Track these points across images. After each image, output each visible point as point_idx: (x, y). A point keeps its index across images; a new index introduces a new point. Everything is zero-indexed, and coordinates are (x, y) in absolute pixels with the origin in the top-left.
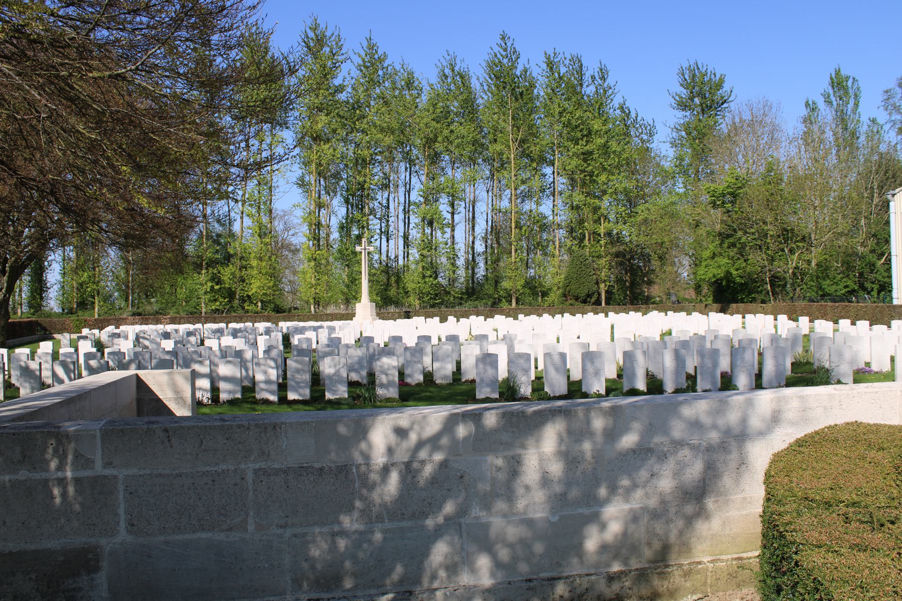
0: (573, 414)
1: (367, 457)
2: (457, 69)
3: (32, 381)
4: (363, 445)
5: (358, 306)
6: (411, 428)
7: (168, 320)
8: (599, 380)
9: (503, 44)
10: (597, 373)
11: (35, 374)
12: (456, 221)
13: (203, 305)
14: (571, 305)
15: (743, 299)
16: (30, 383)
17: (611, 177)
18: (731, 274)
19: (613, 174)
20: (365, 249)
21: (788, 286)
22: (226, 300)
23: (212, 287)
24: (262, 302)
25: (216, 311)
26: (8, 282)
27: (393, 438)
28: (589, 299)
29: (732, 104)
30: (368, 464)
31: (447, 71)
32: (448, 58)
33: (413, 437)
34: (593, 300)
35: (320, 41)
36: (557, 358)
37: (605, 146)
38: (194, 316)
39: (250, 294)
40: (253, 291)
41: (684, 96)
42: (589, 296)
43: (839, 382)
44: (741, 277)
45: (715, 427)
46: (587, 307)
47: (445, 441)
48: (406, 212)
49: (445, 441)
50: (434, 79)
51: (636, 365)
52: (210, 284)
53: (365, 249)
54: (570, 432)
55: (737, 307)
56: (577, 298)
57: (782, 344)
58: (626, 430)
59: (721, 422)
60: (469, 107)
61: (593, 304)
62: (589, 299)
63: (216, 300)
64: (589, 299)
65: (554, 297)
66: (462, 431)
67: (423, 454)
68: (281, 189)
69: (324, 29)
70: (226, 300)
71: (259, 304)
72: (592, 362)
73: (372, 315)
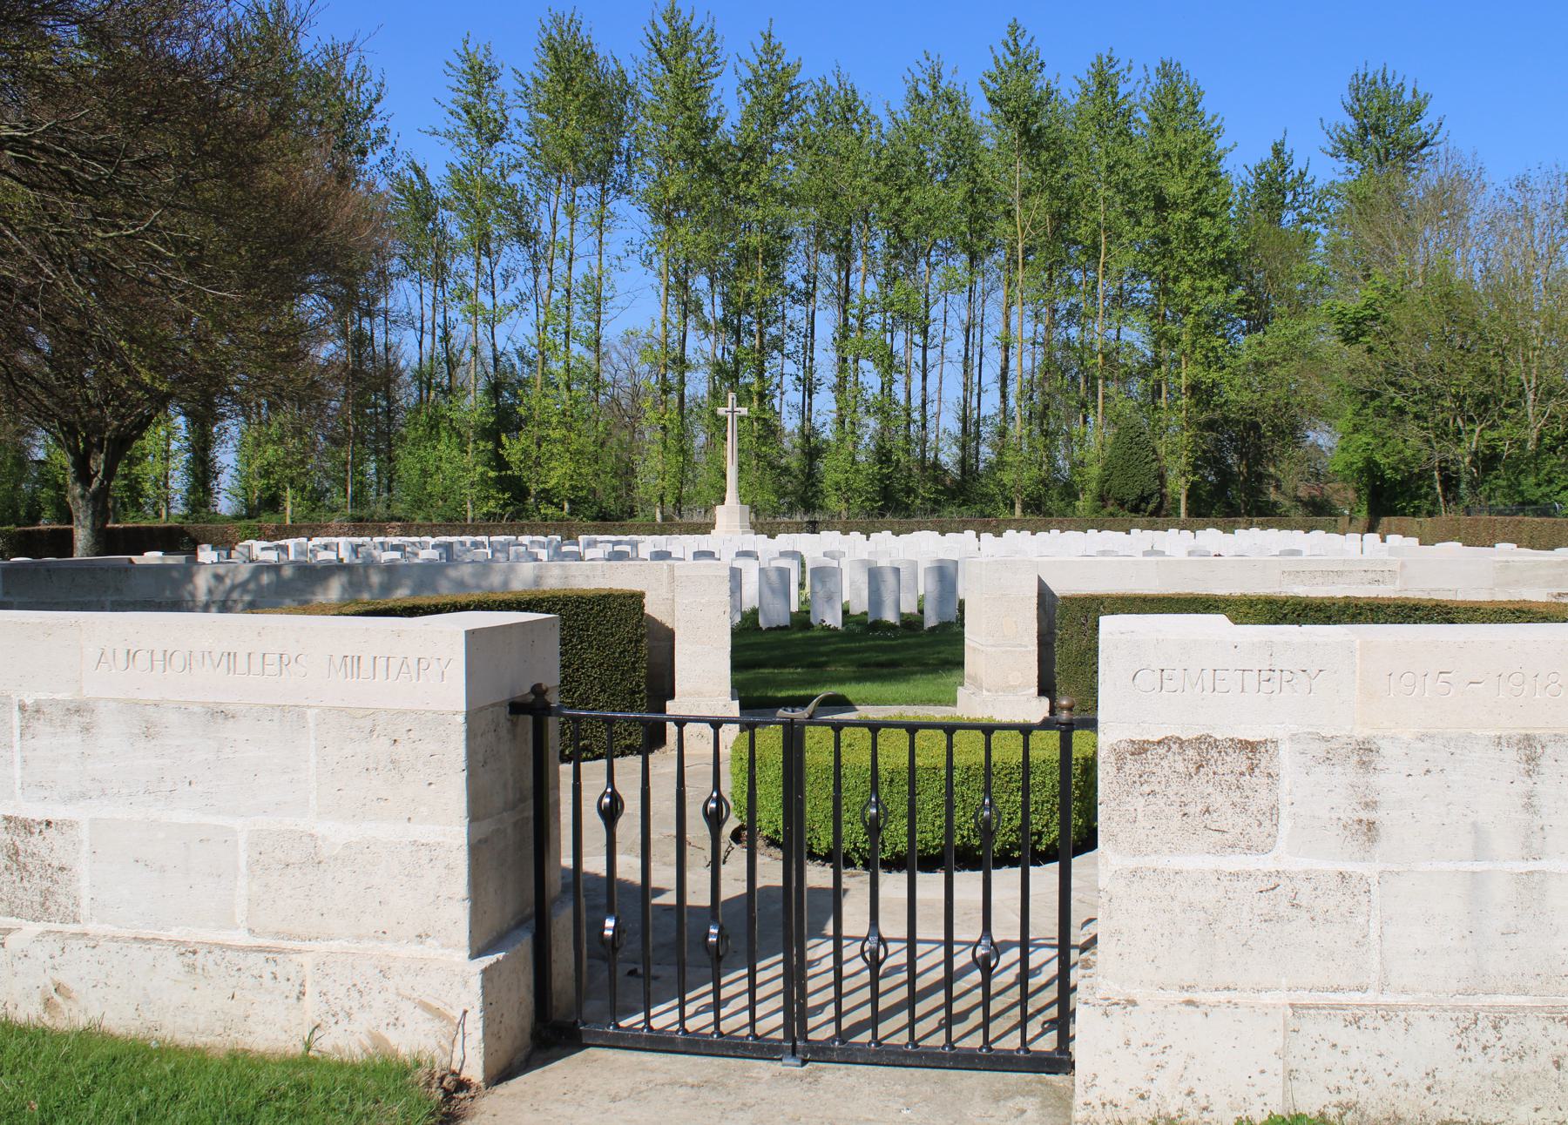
1: (193, 595)
2: (943, 84)
4: (190, 587)
5: (720, 511)
6: (226, 575)
7: (397, 530)
8: (833, 608)
9: (1011, 43)
10: (829, 599)
12: (930, 362)
13: (469, 506)
14: (1111, 514)
15: (1404, 508)
17: (1198, 284)
18: (1377, 465)
19: (1202, 278)
20: (733, 412)
21: (1463, 486)
22: (507, 496)
24: (571, 501)
25: (489, 516)
26: (106, 463)
27: (213, 582)
28: (1143, 505)
29: (1441, 148)
30: (193, 601)
31: (924, 90)
32: (926, 64)
33: (228, 582)
34: (1151, 507)
35: (682, 38)
36: (774, 577)
37: (1191, 228)
38: (454, 523)
40: (553, 482)
41: (1350, 131)
42: (1144, 499)
44: (1396, 469)
45: (478, 587)
46: (1139, 519)
47: (252, 586)
49: (252, 586)
50: (900, 104)
51: (883, 588)
52: (480, 469)
53: (733, 412)
54: (351, 584)
55: (1389, 524)
56: (1121, 504)
58: (398, 586)
59: (484, 584)
60: (962, 148)
61: (1151, 514)
63: (487, 498)
64: (1143, 505)
65: (1084, 503)
66: (265, 579)
67: (235, 595)
68: (617, 301)
69: (688, 20)
70: (507, 496)
71: (566, 506)
72: (823, 583)
73: (742, 527)
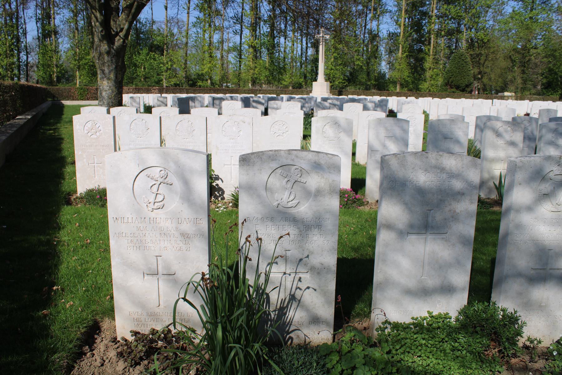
13: (164, 80)
14: (453, 92)
25: (176, 85)
42: (467, 86)
73: (327, 92)
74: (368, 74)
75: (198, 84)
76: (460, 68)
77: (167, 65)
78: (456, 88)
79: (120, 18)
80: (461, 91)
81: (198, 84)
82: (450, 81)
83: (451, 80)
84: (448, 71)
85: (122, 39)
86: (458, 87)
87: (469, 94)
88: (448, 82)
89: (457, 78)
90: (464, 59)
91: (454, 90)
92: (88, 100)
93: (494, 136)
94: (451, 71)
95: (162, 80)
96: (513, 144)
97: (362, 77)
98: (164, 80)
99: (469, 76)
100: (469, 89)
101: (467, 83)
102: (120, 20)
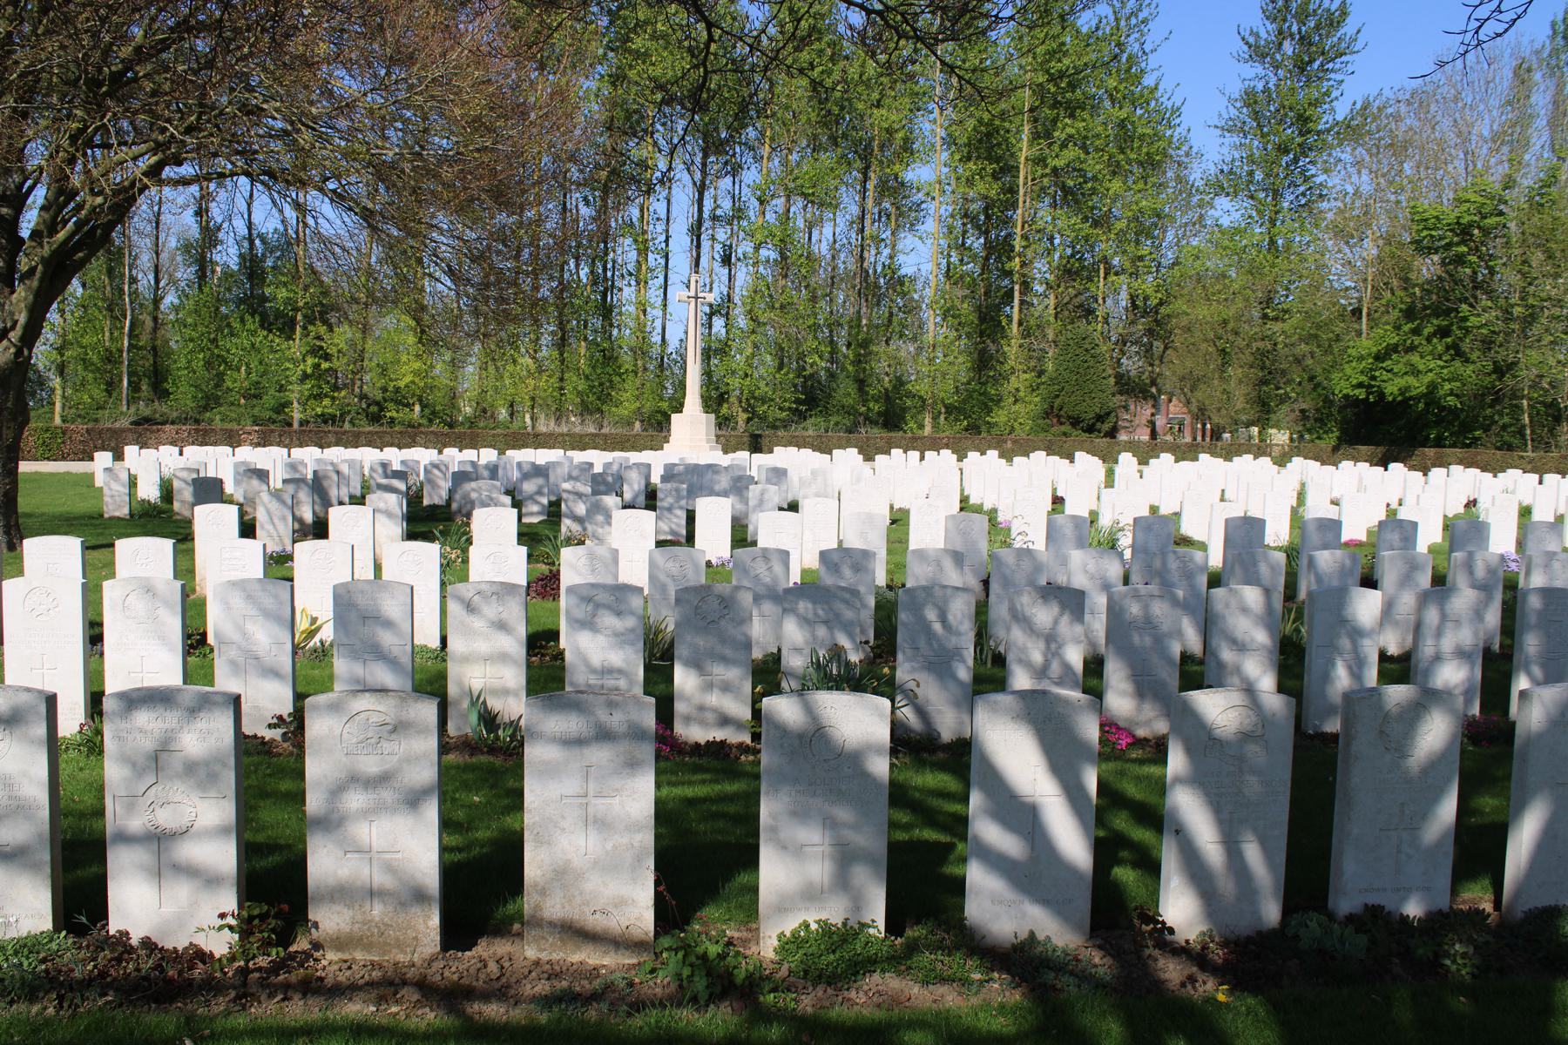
0: (721, 588)
3: (843, 814)
11: (866, 776)
13: (295, 405)
14: (1065, 434)
16: (829, 823)
20: (696, 298)
23: (317, 366)
25: (325, 419)
39: (402, 384)
42: (1100, 418)
43: (1372, 568)
48: (696, 231)
52: (310, 361)
57: (709, 475)
62: (1098, 425)
73: (708, 441)
74: (861, 384)
75: (388, 414)
76: (1081, 370)
77: (302, 367)
78: (1072, 424)
79: (15, 295)
80: (1084, 431)
81: (388, 414)
82: (1056, 405)
83: (1058, 402)
84: (1051, 379)
85: (15, 346)
86: (1075, 422)
87: (1108, 439)
88: (1052, 407)
89: (1073, 398)
90: (1089, 347)
91: (1066, 428)
92: (64, 458)
93: (464, 613)
94: (1056, 378)
95: (288, 404)
96: (502, 626)
97: (846, 391)
98: (295, 405)
99: (1103, 392)
100: (1106, 427)
101: (1098, 410)
102: (14, 301)
